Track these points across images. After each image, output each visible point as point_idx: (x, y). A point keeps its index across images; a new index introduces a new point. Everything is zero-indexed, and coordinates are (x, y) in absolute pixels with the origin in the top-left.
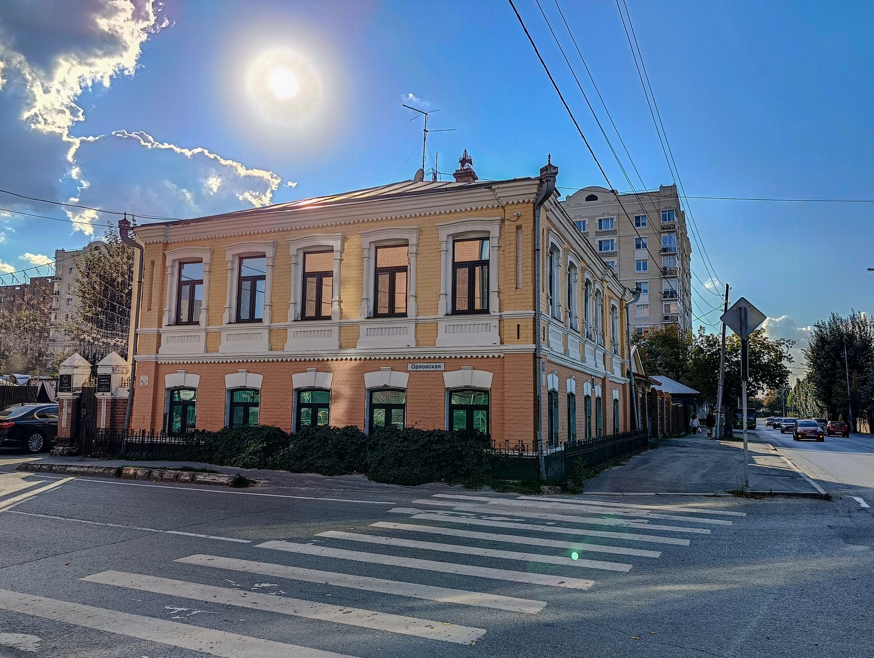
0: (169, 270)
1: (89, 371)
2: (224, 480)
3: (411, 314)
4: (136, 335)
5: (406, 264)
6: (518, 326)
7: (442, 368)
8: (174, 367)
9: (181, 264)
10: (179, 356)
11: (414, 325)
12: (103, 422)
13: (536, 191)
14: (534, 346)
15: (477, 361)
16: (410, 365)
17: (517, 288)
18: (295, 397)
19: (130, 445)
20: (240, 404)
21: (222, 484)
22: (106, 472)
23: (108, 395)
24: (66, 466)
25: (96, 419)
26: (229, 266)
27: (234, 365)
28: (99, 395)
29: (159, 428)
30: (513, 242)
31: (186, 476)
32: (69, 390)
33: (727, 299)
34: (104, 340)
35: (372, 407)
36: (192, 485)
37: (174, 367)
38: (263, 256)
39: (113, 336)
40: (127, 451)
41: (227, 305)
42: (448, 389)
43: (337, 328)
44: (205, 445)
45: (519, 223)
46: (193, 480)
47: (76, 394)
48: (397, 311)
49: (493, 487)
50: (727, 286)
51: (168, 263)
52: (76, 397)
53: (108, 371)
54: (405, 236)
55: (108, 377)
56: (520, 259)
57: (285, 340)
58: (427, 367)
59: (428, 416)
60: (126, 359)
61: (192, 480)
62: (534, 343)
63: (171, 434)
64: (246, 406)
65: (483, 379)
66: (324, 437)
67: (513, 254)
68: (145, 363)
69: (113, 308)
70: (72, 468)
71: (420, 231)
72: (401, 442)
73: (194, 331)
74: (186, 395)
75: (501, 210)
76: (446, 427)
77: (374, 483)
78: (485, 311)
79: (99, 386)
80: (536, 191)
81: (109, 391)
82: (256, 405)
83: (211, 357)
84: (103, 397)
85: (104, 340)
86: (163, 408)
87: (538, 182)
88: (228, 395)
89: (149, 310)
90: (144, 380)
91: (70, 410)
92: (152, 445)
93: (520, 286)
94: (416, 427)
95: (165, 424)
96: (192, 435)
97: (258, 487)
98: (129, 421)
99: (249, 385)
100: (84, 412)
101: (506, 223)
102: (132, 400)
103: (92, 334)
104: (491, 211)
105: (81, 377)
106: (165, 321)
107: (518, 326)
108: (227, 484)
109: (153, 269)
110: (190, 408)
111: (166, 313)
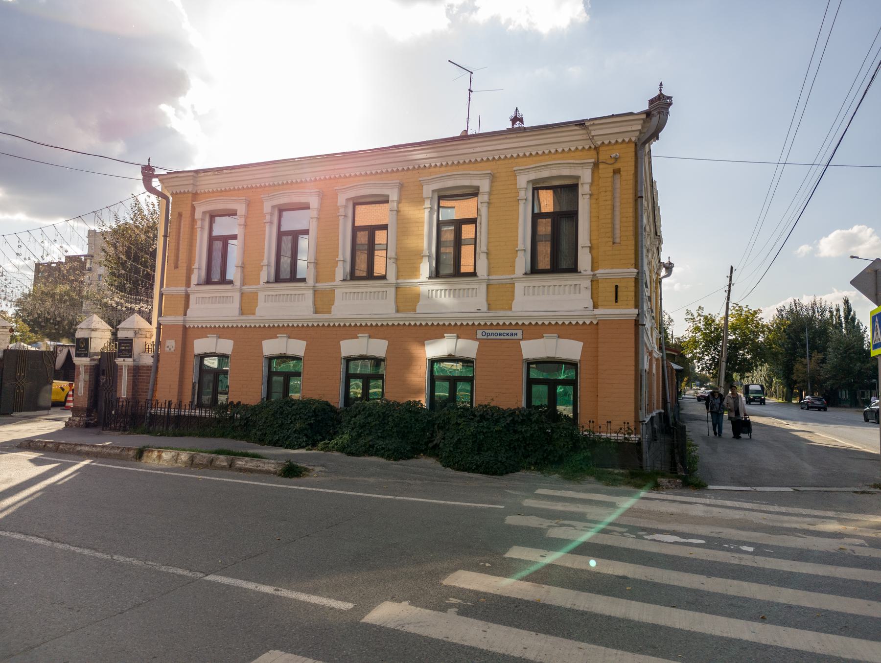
0: (199, 223)
1: (108, 335)
2: (270, 466)
3: (482, 271)
4: (161, 295)
5: (475, 216)
6: (617, 287)
7: (520, 336)
8: (204, 331)
9: (212, 216)
10: (208, 319)
11: (485, 286)
12: (124, 390)
13: (640, 127)
14: (636, 311)
15: (564, 329)
16: (479, 332)
17: (614, 243)
18: (343, 367)
19: (153, 417)
20: (280, 372)
21: (268, 472)
22: (124, 453)
23: (129, 361)
24: (76, 445)
25: (116, 387)
26: (268, 218)
27: (272, 331)
28: (119, 361)
29: (187, 398)
30: (610, 189)
31: (222, 461)
32: (86, 355)
33: (731, 280)
34: (129, 305)
35: (349, 377)
36: (230, 473)
37: (204, 331)
38: (306, 207)
39: (137, 301)
40: (150, 424)
41: (265, 262)
42: (526, 360)
43: (393, 289)
44: (241, 419)
45: (617, 166)
46: (231, 466)
47: (94, 360)
48: (463, 270)
49: (599, 479)
50: (732, 268)
51: (198, 215)
52: (94, 363)
53: (130, 334)
54: (475, 183)
55: (129, 342)
56: (617, 209)
57: (332, 301)
58: (500, 334)
59: (504, 392)
60: (149, 320)
61: (230, 466)
62: (636, 307)
63: (200, 406)
64: (288, 376)
65: (571, 349)
66: (383, 413)
67: (609, 203)
68: (169, 327)
69: (137, 271)
70: (83, 448)
71: (493, 178)
72: (479, 422)
73: (228, 291)
74: (212, 363)
75: (594, 153)
76: (524, 404)
77: (450, 472)
78: (573, 269)
79: (120, 351)
80: (640, 127)
81: (130, 357)
82: (298, 374)
83: (248, 320)
84: (124, 363)
85: (129, 305)
86: (192, 376)
87: (644, 116)
88: (265, 364)
89: (176, 267)
90: (171, 345)
91: (87, 378)
92: (179, 417)
93: (618, 240)
94: (492, 404)
95: (193, 394)
96: (225, 407)
97: (312, 478)
98: (154, 390)
99: (291, 352)
100: (103, 379)
101: (601, 166)
102: (157, 367)
103: (114, 299)
104: (581, 153)
105: (100, 338)
106: (194, 279)
107: (617, 287)
108: (275, 473)
109: (180, 222)
110: (221, 377)
111: (196, 271)
